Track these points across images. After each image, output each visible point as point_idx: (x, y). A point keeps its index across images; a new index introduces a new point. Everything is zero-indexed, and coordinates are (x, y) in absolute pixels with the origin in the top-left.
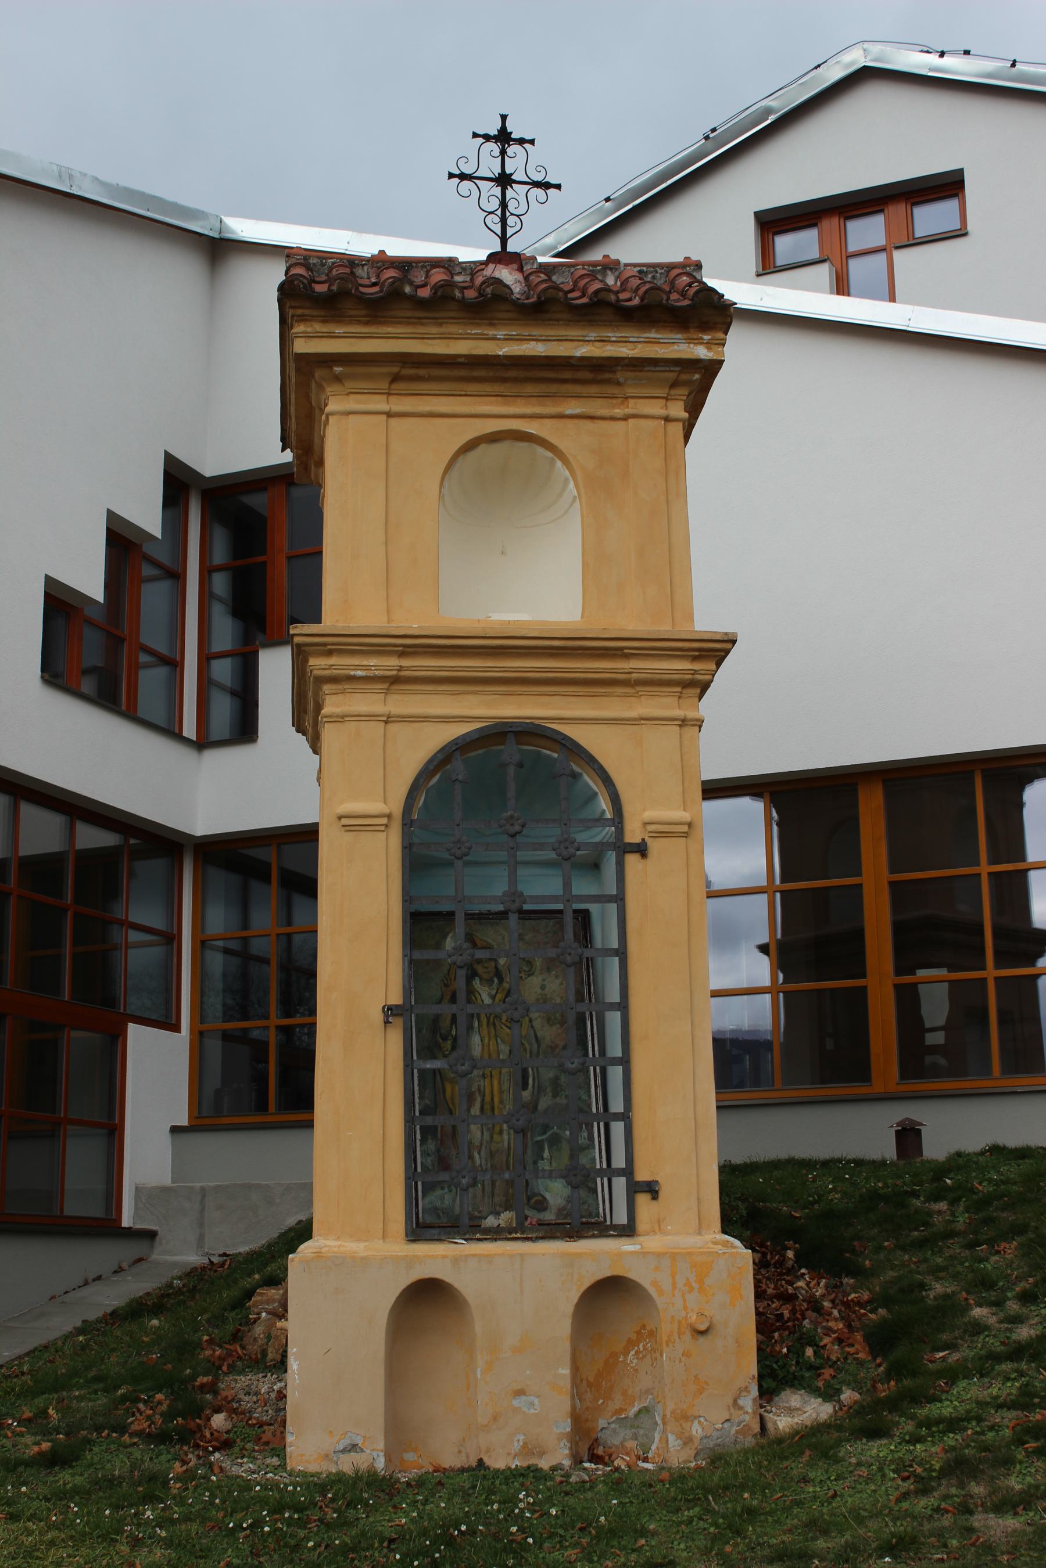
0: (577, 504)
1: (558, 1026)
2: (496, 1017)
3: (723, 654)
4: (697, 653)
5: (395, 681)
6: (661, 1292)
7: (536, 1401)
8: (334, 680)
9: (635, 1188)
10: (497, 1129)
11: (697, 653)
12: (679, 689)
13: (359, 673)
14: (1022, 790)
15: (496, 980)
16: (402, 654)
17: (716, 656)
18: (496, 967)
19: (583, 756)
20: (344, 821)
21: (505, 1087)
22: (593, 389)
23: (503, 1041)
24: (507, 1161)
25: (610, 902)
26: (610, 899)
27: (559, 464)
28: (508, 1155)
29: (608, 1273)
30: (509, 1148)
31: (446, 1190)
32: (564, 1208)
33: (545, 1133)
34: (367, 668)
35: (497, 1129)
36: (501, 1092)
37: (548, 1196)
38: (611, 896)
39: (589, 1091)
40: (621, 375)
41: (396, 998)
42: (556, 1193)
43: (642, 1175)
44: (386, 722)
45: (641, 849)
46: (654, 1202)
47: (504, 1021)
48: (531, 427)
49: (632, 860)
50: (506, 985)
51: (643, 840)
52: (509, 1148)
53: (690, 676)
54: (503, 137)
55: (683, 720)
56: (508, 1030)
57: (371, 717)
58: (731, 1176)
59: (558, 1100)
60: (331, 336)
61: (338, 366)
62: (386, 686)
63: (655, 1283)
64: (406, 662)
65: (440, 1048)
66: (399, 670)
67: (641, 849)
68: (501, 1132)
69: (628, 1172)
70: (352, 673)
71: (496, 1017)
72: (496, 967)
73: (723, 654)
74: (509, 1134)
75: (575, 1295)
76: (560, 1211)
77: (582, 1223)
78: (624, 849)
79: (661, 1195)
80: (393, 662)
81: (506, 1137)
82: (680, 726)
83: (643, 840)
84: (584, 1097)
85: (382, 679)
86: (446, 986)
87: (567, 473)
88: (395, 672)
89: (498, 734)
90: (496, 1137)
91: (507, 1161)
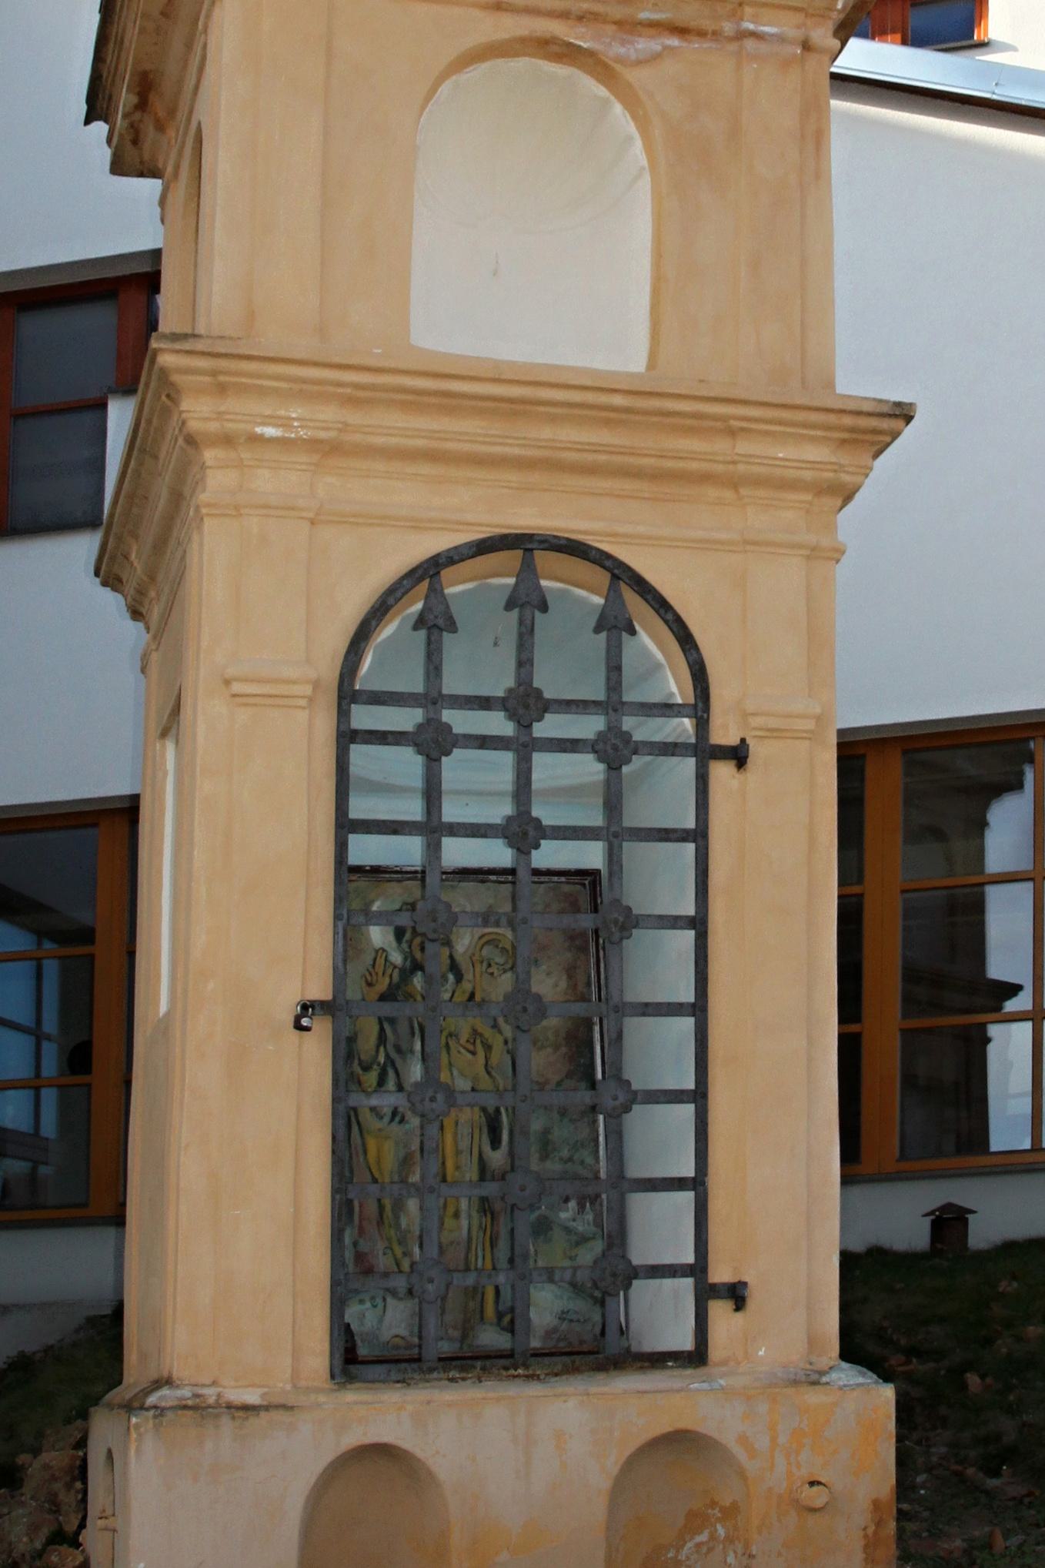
0: (647, 178)
1: (550, 1050)
2: (450, 1035)
3: (888, 439)
4: (846, 435)
5: (329, 450)
6: (752, 1453)
8: (227, 440)
9: (706, 1293)
10: (451, 1210)
11: (846, 435)
12: (808, 497)
13: (270, 431)
14: (985, 807)
15: (451, 977)
17: (873, 443)
18: (451, 957)
19: (649, 597)
20: (237, 688)
21: (464, 1144)
23: (462, 1074)
24: (467, 1258)
25: (684, 840)
26: (683, 836)
27: (618, 108)
28: (469, 1248)
30: (470, 1239)
31: (368, 1305)
32: (555, 1330)
35: (451, 1210)
36: (458, 1153)
38: (686, 831)
39: (597, 1151)
41: (320, 989)
42: (546, 1306)
43: (720, 1273)
44: (312, 522)
45: (738, 755)
46: (739, 1315)
47: (463, 1041)
48: (581, 37)
49: (722, 772)
50: (467, 986)
51: (743, 740)
52: (470, 1239)
53: (831, 475)
55: (813, 549)
56: (469, 1056)
58: (859, 1268)
59: (548, 1164)
62: (315, 458)
63: (743, 1440)
64: (354, 417)
65: (359, 1083)
66: (340, 430)
67: (738, 755)
68: (457, 1215)
69: (698, 1269)
70: (258, 430)
71: (450, 1035)
72: (451, 957)
73: (888, 439)
74: (470, 1217)
75: (614, 1462)
76: (549, 1334)
77: (599, 1350)
78: (705, 752)
80: (329, 413)
81: (465, 1223)
82: (808, 557)
83: (743, 740)
84: (589, 1160)
85: (313, 445)
86: (370, 984)
87: (632, 128)
88: (332, 434)
90: (449, 1222)
91: (467, 1258)
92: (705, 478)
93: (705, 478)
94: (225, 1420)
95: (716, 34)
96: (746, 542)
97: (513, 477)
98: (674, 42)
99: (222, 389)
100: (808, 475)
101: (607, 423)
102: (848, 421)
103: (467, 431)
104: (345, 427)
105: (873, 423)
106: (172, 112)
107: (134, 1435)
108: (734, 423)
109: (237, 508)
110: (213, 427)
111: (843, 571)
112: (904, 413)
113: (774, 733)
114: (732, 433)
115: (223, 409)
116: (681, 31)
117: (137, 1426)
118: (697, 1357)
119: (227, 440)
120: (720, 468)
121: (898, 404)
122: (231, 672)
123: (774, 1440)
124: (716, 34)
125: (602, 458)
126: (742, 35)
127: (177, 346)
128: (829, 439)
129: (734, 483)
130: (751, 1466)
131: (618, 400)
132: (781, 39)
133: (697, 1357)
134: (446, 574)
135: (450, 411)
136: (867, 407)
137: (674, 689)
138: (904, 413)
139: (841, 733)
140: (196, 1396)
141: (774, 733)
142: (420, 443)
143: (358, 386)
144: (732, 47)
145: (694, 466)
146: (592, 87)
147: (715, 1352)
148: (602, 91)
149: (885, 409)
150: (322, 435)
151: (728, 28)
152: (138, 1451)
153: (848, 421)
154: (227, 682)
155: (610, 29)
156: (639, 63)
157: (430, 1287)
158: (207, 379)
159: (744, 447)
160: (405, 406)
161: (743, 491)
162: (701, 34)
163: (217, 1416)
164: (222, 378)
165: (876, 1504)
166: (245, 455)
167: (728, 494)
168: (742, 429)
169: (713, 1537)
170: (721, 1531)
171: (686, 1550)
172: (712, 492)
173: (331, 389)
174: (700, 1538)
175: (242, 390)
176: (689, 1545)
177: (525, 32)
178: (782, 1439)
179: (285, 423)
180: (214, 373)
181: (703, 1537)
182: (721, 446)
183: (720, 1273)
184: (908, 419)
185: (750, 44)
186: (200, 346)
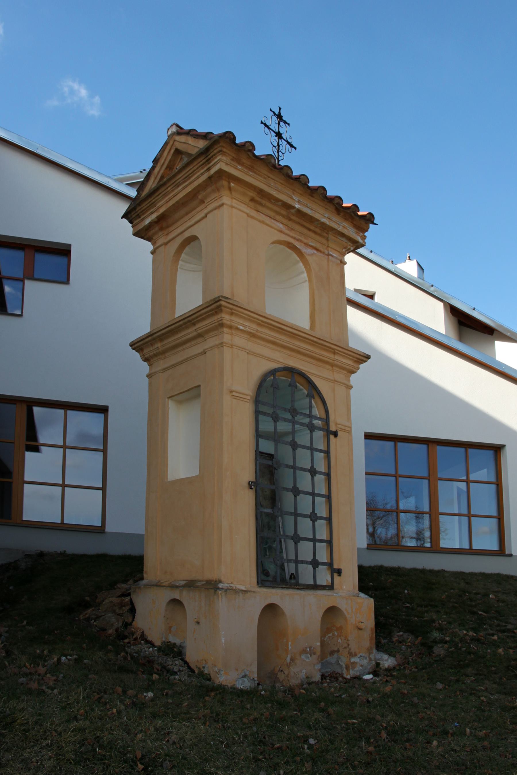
0: (307, 284)
4: (356, 360)
5: (253, 335)
7: (361, 654)
8: (230, 327)
11: (356, 360)
13: (241, 327)
16: (259, 325)
20: (234, 394)
22: (318, 238)
27: (301, 264)
29: (331, 605)
33: (266, 545)
34: (245, 326)
37: (269, 571)
40: (331, 236)
43: (335, 566)
46: (339, 577)
48: (298, 245)
54: (280, 117)
57: (243, 349)
60: (236, 168)
61: (233, 183)
62: (249, 337)
64: (259, 329)
67: (335, 434)
69: (330, 565)
70: (239, 326)
79: (342, 574)
80: (254, 326)
85: (249, 333)
89: (290, 371)
92: (327, 363)
93: (327, 363)
94: (240, 594)
95: (324, 253)
96: (335, 381)
97: (289, 352)
98: (315, 252)
99: (232, 314)
100: (348, 367)
101: (310, 344)
102: (358, 356)
103: (283, 339)
104: (257, 331)
105: (362, 358)
106: (168, 227)
107: (220, 596)
108: (336, 351)
109: (232, 345)
110: (229, 323)
111: (352, 391)
112: (368, 357)
113: (342, 430)
114: (334, 353)
115: (232, 319)
116: (317, 250)
117: (221, 593)
118: (331, 587)
119: (230, 327)
120: (331, 361)
121: (368, 355)
122: (234, 389)
123: (352, 610)
124: (324, 253)
125: (308, 352)
126: (329, 255)
127: (226, 300)
128: (352, 360)
129: (332, 365)
130: (348, 617)
131: (315, 339)
132: (336, 258)
133: (331, 587)
134: (277, 374)
135: (280, 333)
136: (362, 354)
137: (318, 414)
138: (368, 357)
139: (365, 433)
140: (230, 586)
141: (342, 430)
142: (272, 339)
143: (262, 321)
144: (327, 257)
145: (326, 359)
146: (295, 256)
147: (335, 587)
148: (298, 259)
149: (365, 355)
150: (252, 331)
151: (326, 252)
152: (221, 600)
153: (358, 356)
154: (231, 392)
155: (303, 244)
156: (309, 255)
157: (278, 562)
158: (230, 310)
159: (337, 357)
160: (270, 329)
161: (334, 368)
162: (321, 252)
163: (239, 592)
164: (233, 311)
165: (371, 628)
166: (233, 332)
167: (330, 367)
168: (338, 353)
169: (334, 634)
170: (336, 633)
171: (326, 638)
172: (328, 367)
173: (256, 320)
174: (329, 635)
175: (237, 315)
176: (327, 636)
177: (286, 240)
178: (354, 610)
179: (245, 326)
180: (231, 309)
181: (331, 635)
182: (332, 356)
183: (335, 566)
184: (369, 358)
185: (330, 257)
186: (231, 302)
